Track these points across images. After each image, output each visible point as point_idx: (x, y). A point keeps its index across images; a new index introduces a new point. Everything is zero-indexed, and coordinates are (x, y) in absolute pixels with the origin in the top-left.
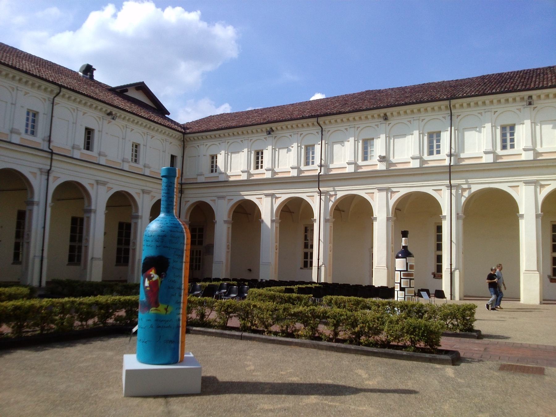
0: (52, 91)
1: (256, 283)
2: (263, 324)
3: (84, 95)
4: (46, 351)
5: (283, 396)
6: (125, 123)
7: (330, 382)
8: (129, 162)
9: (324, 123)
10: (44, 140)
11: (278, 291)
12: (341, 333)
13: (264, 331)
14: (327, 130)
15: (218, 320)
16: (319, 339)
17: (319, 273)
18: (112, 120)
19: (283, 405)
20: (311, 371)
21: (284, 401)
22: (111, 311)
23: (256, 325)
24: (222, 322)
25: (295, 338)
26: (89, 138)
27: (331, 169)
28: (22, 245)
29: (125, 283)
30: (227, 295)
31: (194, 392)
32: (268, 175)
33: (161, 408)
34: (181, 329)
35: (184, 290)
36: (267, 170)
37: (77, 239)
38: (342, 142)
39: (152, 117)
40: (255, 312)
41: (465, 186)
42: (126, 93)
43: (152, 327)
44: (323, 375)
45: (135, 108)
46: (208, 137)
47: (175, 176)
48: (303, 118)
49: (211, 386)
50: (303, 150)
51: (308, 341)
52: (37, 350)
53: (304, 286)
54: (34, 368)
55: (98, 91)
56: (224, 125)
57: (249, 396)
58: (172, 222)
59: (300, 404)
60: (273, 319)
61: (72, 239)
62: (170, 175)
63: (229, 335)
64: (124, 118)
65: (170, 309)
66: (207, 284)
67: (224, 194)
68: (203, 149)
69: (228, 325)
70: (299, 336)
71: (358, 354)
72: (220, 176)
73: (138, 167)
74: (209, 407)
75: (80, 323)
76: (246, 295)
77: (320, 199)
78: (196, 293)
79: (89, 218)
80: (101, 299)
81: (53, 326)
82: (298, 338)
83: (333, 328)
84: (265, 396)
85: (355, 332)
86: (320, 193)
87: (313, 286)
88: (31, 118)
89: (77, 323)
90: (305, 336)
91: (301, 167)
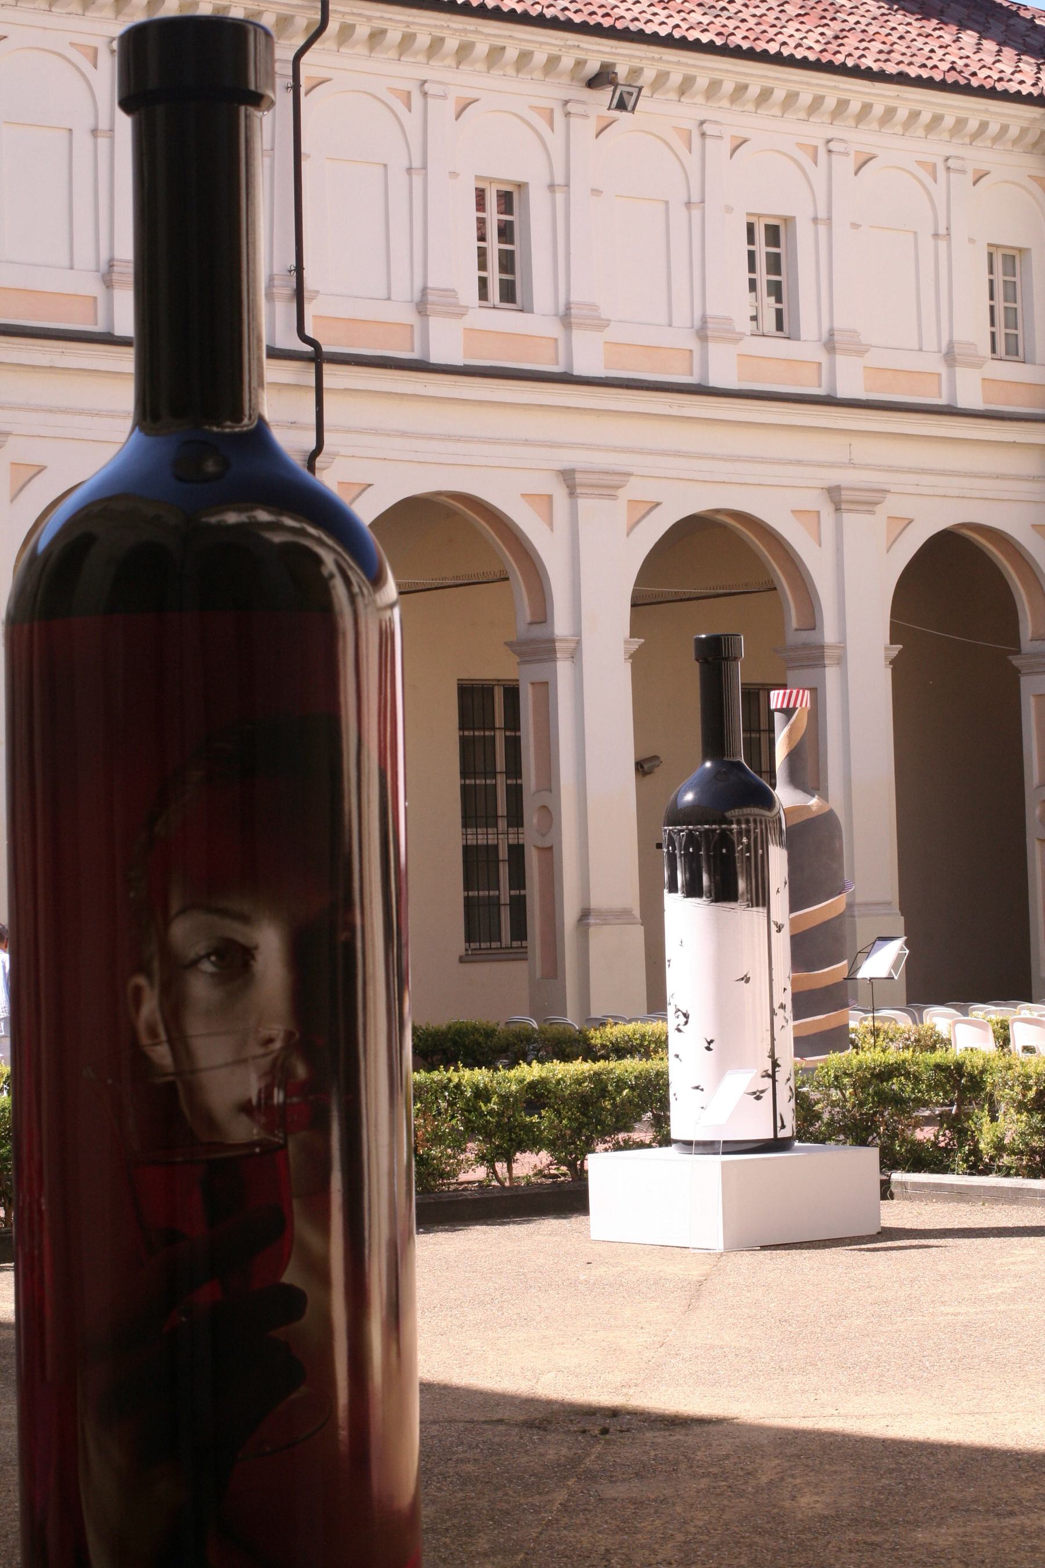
6: (689, 112)
18: (617, 114)
37: (502, 809)
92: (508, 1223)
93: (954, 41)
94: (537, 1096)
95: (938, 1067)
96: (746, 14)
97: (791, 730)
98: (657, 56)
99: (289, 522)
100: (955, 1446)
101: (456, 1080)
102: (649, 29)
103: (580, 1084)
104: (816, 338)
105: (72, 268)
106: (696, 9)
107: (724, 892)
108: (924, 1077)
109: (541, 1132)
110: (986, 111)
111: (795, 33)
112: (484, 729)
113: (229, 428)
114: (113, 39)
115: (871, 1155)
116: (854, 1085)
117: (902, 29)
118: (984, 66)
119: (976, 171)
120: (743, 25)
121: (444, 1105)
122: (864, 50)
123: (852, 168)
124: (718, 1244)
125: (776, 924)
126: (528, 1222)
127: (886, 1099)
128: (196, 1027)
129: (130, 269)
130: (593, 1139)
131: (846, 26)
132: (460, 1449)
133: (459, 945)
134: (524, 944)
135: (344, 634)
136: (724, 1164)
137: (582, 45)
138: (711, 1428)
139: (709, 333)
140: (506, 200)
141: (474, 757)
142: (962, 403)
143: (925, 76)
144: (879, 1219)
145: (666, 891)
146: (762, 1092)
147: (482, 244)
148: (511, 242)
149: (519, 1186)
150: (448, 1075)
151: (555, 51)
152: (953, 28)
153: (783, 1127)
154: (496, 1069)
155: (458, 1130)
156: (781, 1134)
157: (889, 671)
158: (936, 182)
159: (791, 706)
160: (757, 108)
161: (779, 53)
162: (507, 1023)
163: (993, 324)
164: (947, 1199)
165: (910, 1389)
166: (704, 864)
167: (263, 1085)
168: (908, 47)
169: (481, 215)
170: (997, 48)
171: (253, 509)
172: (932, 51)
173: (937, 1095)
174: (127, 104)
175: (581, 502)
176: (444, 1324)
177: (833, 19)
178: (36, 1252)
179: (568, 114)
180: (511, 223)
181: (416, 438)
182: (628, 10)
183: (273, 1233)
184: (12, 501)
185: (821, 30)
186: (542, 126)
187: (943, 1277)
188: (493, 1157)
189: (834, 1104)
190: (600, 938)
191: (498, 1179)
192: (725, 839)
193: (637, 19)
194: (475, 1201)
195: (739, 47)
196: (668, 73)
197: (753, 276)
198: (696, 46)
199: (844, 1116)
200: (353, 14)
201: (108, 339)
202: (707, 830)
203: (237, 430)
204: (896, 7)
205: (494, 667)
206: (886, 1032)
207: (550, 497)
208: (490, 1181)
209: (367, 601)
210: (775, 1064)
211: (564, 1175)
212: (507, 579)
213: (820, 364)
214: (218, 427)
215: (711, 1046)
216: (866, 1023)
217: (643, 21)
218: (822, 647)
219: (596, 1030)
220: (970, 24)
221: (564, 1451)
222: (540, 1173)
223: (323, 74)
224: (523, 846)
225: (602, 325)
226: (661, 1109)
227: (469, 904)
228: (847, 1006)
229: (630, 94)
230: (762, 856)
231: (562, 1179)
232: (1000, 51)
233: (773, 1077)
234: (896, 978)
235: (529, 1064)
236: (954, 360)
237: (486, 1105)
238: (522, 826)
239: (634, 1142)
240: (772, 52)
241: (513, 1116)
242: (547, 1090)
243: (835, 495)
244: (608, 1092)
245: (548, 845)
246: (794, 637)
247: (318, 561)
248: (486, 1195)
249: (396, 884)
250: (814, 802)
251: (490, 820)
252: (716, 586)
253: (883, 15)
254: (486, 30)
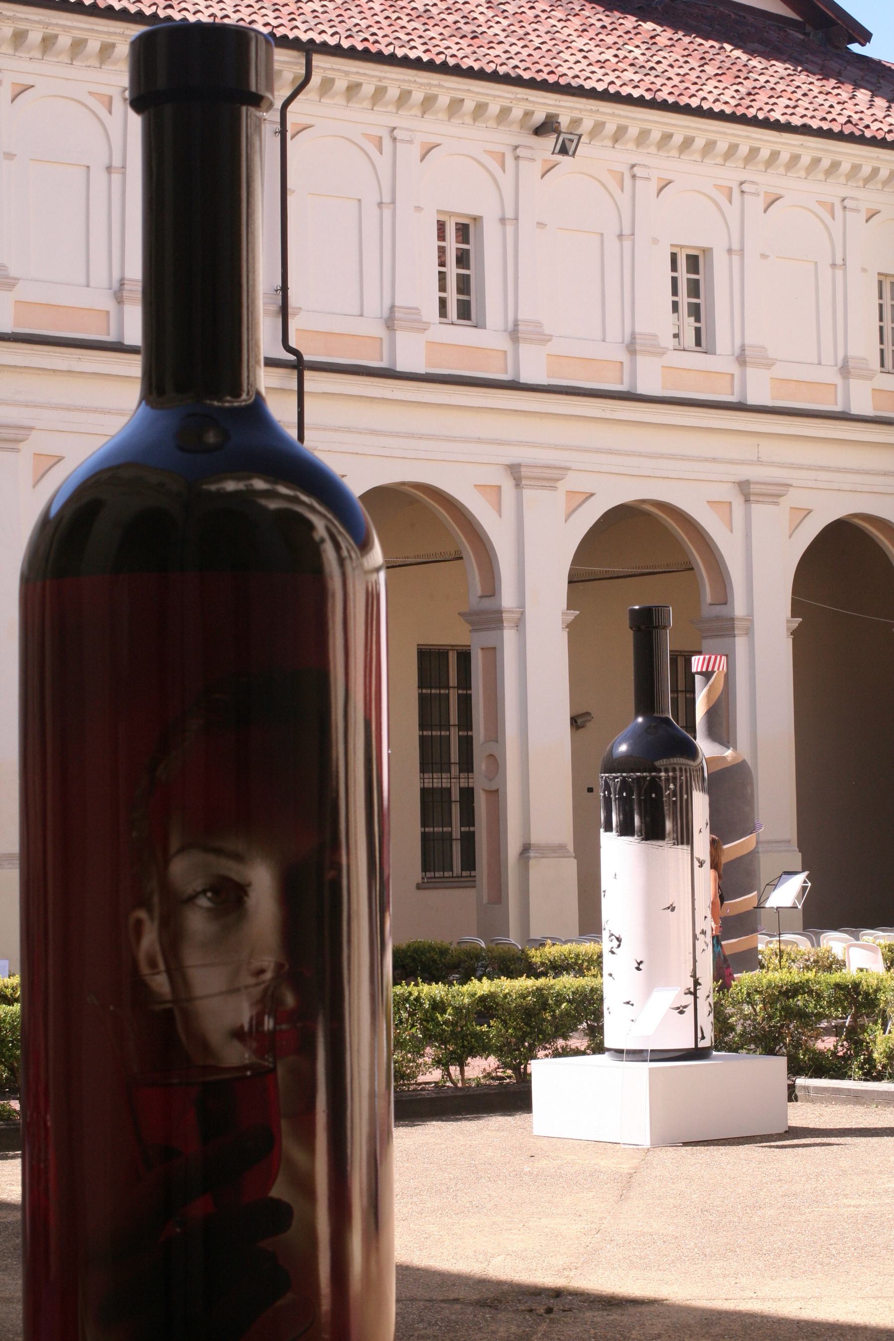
6: (623, 156)
18: (560, 158)
37: (454, 756)
73: (479, 347)
92: (460, 1120)
93: (850, 99)
94: (486, 1008)
95: (838, 986)
96: (671, 73)
97: (709, 691)
98: (594, 108)
99: (283, 490)
100: (861, 1327)
101: (416, 994)
102: (588, 85)
103: (524, 998)
104: (730, 353)
105: (88, 286)
106: (628, 68)
107: (653, 832)
108: (826, 994)
109: (490, 1040)
110: (878, 158)
111: (714, 90)
112: (440, 688)
113: (229, 403)
114: (125, 89)
115: (780, 1063)
116: (763, 1001)
117: (805, 88)
118: (876, 120)
119: (868, 210)
120: (669, 83)
121: (405, 1015)
122: (773, 104)
123: (762, 207)
124: (645, 1140)
125: (698, 860)
126: (478, 1118)
127: (791, 1014)
128: (192, 958)
129: (139, 288)
130: (535, 1046)
131: (758, 84)
132: (421, 1326)
134: (473, 873)
135: (333, 595)
136: (651, 1070)
137: (531, 98)
138: (643, 1309)
139: (638, 348)
140: (463, 231)
141: (430, 712)
142: (855, 410)
143: (825, 128)
144: (787, 1119)
145: (602, 830)
146: (685, 1007)
147: (442, 269)
148: (467, 267)
149: (470, 1087)
150: (409, 989)
151: (507, 103)
152: (849, 87)
153: (703, 1038)
154: (451, 984)
155: (417, 1037)
156: (701, 1044)
157: (790, 641)
158: (833, 219)
159: (710, 669)
160: (680, 154)
161: (700, 107)
162: (459, 943)
163: (882, 342)
164: (844, 1102)
165: (820, 1275)
166: (636, 807)
167: (254, 1013)
168: (811, 103)
169: (442, 244)
170: (887, 104)
171: (250, 478)
172: (831, 106)
173: (837, 1010)
174: (138, 103)
175: (527, 493)
176: (405, 1210)
177: (747, 78)
178: (42, 1166)
179: (517, 158)
180: (468, 251)
181: (384, 435)
182: (570, 68)
183: (263, 1152)
184: (34, 486)
185: (735, 87)
186: (494, 167)
187: (844, 1172)
188: (448, 1062)
189: (746, 1018)
190: (539, 869)
191: (452, 1081)
192: (655, 785)
193: (577, 76)
194: (431, 1100)
195: (665, 101)
196: (604, 124)
197: (675, 299)
198: (629, 100)
199: (755, 1028)
200: (334, 69)
201: (118, 348)
202: (638, 777)
203: (236, 404)
204: (799, 69)
205: (450, 634)
206: (789, 954)
207: (499, 488)
208: (445, 1082)
209: (354, 565)
210: (697, 983)
211: (510, 1077)
212: (461, 558)
213: (733, 375)
214: (218, 401)
215: (641, 967)
216: (771, 946)
217: (583, 78)
218: (732, 619)
219: (536, 950)
220: (864, 84)
221: (514, 1329)
222: (488, 1076)
223: (307, 121)
224: (472, 789)
225: (545, 339)
226: (595, 1020)
227: (425, 838)
228: (757, 931)
229: (572, 141)
230: (687, 800)
231: (508, 1081)
232: (889, 107)
233: (694, 994)
234: (800, 907)
235: (480, 980)
236: (848, 373)
237: (442, 1016)
238: (472, 772)
239: (571, 1050)
240: (694, 106)
241: (466, 1025)
242: (495, 1003)
243: (745, 489)
244: (549, 1005)
245: (494, 788)
246: (707, 611)
247: (311, 527)
248: (442, 1095)
249: (379, 827)
250: (729, 753)
251: (445, 767)
252: (642, 566)
253: (789, 75)
254: (447, 84)
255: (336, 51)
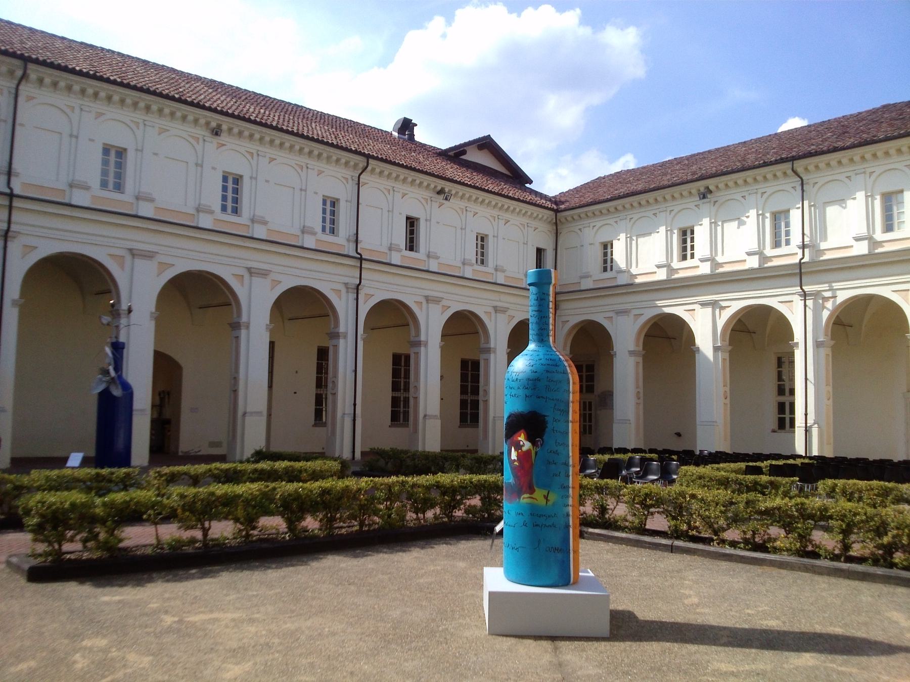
0: (356, 165)
1: (689, 457)
2: (710, 527)
3: (402, 166)
4: (369, 558)
5: (753, 650)
6: (463, 204)
7: (838, 630)
8: (472, 265)
9: (806, 169)
10: (348, 240)
11: (732, 471)
12: (856, 546)
13: (712, 540)
14: (812, 182)
15: (630, 518)
16: (815, 555)
17: (808, 438)
18: (444, 201)
19: (754, 667)
20: (802, 610)
21: (755, 660)
22: (458, 498)
23: (696, 528)
24: (637, 521)
25: (769, 552)
26: (412, 232)
27: (823, 252)
28: (326, 398)
29: (476, 455)
30: (642, 475)
31: (592, 635)
32: (705, 269)
33: (547, 658)
34: (571, 530)
35: (574, 466)
36: (702, 261)
38: (841, 202)
39: (505, 190)
40: (695, 506)
41: (828, 294)
42: (463, 157)
43: (525, 525)
44: (824, 618)
45: (478, 179)
46: (597, 213)
47: (550, 283)
48: (766, 164)
49: (625, 627)
50: (768, 222)
51: (793, 559)
52: (356, 556)
53: (781, 462)
54: (353, 583)
55: (421, 159)
56: (623, 190)
57: (693, 648)
58: (548, 357)
59: (785, 666)
60: (727, 519)
61: (395, 387)
62: (542, 281)
63: (650, 543)
64: (462, 197)
65: (552, 497)
66: (607, 457)
67: (628, 306)
68: (588, 233)
69: (647, 527)
70: (776, 550)
71: (890, 583)
72: (620, 276)
74: (626, 660)
75: (414, 516)
76: (675, 477)
77: (805, 306)
78: (589, 471)
79: (417, 354)
80: (445, 478)
81: (376, 519)
82: (775, 553)
83: (841, 537)
84: (720, 648)
85: (882, 544)
86: (805, 295)
87: (798, 462)
88: (230, 185)
89: (410, 516)
90: (787, 550)
91: (672, 264)
133: (389, 422)
198: (467, 185)
205: (469, 356)
246: (482, 346)
255: (377, 158)
